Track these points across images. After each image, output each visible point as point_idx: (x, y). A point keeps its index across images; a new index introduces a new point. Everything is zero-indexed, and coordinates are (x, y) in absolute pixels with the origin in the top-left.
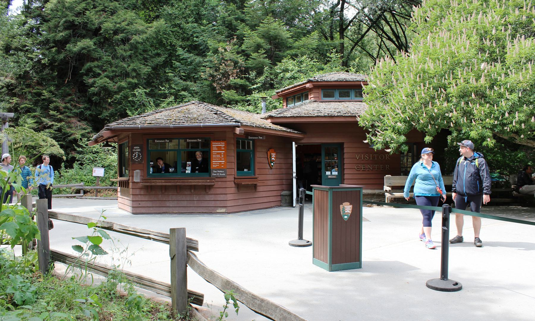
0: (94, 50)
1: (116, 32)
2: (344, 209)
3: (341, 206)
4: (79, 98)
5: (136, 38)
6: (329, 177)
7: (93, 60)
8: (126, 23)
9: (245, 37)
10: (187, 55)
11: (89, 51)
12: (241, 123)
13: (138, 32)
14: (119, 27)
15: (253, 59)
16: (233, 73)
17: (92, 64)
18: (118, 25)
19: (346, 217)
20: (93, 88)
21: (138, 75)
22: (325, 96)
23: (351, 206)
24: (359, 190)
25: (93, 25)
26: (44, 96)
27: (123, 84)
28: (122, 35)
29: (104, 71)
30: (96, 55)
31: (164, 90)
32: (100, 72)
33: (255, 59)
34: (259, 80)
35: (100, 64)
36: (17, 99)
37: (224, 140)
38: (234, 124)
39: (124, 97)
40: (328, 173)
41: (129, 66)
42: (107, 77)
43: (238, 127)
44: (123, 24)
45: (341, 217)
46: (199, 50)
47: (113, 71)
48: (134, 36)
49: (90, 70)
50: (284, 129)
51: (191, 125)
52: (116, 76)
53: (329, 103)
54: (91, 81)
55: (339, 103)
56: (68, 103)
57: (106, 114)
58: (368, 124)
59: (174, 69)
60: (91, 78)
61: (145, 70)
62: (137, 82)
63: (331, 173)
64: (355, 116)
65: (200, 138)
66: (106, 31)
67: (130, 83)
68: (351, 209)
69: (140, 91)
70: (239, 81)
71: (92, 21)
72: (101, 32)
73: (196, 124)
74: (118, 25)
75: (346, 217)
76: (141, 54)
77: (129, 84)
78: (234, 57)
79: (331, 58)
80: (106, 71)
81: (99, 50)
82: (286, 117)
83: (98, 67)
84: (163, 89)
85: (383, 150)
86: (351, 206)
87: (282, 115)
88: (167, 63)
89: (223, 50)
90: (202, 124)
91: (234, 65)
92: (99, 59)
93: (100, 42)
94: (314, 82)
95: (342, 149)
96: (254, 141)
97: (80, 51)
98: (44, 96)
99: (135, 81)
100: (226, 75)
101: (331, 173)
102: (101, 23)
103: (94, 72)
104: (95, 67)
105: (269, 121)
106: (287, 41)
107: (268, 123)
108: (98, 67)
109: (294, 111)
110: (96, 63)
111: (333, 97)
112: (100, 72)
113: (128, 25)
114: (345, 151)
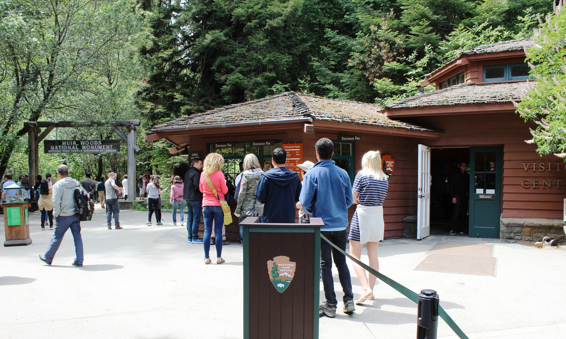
0: (225, 42)
1: (249, 19)
2: (275, 268)
3: (270, 264)
4: (215, 99)
5: (274, 23)
6: (481, 197)
7: (225, 54)
8: (259, 6)
9: (403, 5)
10: (339, 38)
11: (219, 43)
12: (313, 118)
13: (272, 16)
14: (252, 12)
15: (414, 35)
16: (388, 58)
17: (223, 59)
18: (250, 10)
19: (281, 285)
20: (224, 87)
21: (276, 68)
22: (489, 76)
23: (293, 265)
24: (312, 231)
25: (223, 12)
26: (176, 99)
27: (259, 79)
28: (255, 21)
29: (238, 66)
30: (228, 48)
31: (303, 84)
32: (233, 67)
33: (418, 36)
34: (418, 63)
35: (232, 58)
36: (152, 104)
37: (299, 142)
38: (302, 118)
39: (260, 94)
40: (480, 191)
41: (265, 57)
42: (241, 72)
43: (308, 122)
44: (256, 8)
45: (271, 286)
46: (350, 30)
47: (248, 65)
48: (268, 20)
49: (221, 66)
50: (404, 125)
51: (252, 122)
52: (249, 72)
53: (491, 86)
54: (223, 78)
55: (504, 85)
56: (202, 105)
57: (47, 106)
58: (532, 113)
59: (322, 57)
60: (223, 75)
61: (285, 59)
62: (274, 75)
63: (485, 192)
64: (510, 103)
65: (268, 141)
66: (238, 17)
67: (267, 78)
68: (293, 271)
69: (278, 86)
70: (394, 65)
71: (221, 8)
72: (232, 20)
73: (254, 121)
74: (250, 10)
75: (281, 285)
76: (283, 42)
77: (266, 79)
78: (391, 35)
79: (523, 22)
80: (239, 66)
81: (232, 42)
82: (408, 109)
83: (230, 61)
84: (302, 82)
85: (552, 154)
86: (293, 265)
87: (404, 105)
88: (315, 50)
89: (376, 29)
90: (260, 121)
91: (391, 47)
92: (231, 53)
93: (234, 34)
94: (470, 56)
95: (502, 154)
96: (354, 142)
97: (209, 44)
98: (176, 99)
99: (273, 74)
100: (379, 60)
101: (485, 192)
102: (232, 10)
103: (226, 68)
104: (227, 62)
105: (386, 114)
106: (465, 6)
107: (383, 119)
108: (230, 61)
109: (425, 99)
110: (228, 57)
111: (502, 76)
112: (233, 67)
113: (262, 7)
114: (505, 158)
